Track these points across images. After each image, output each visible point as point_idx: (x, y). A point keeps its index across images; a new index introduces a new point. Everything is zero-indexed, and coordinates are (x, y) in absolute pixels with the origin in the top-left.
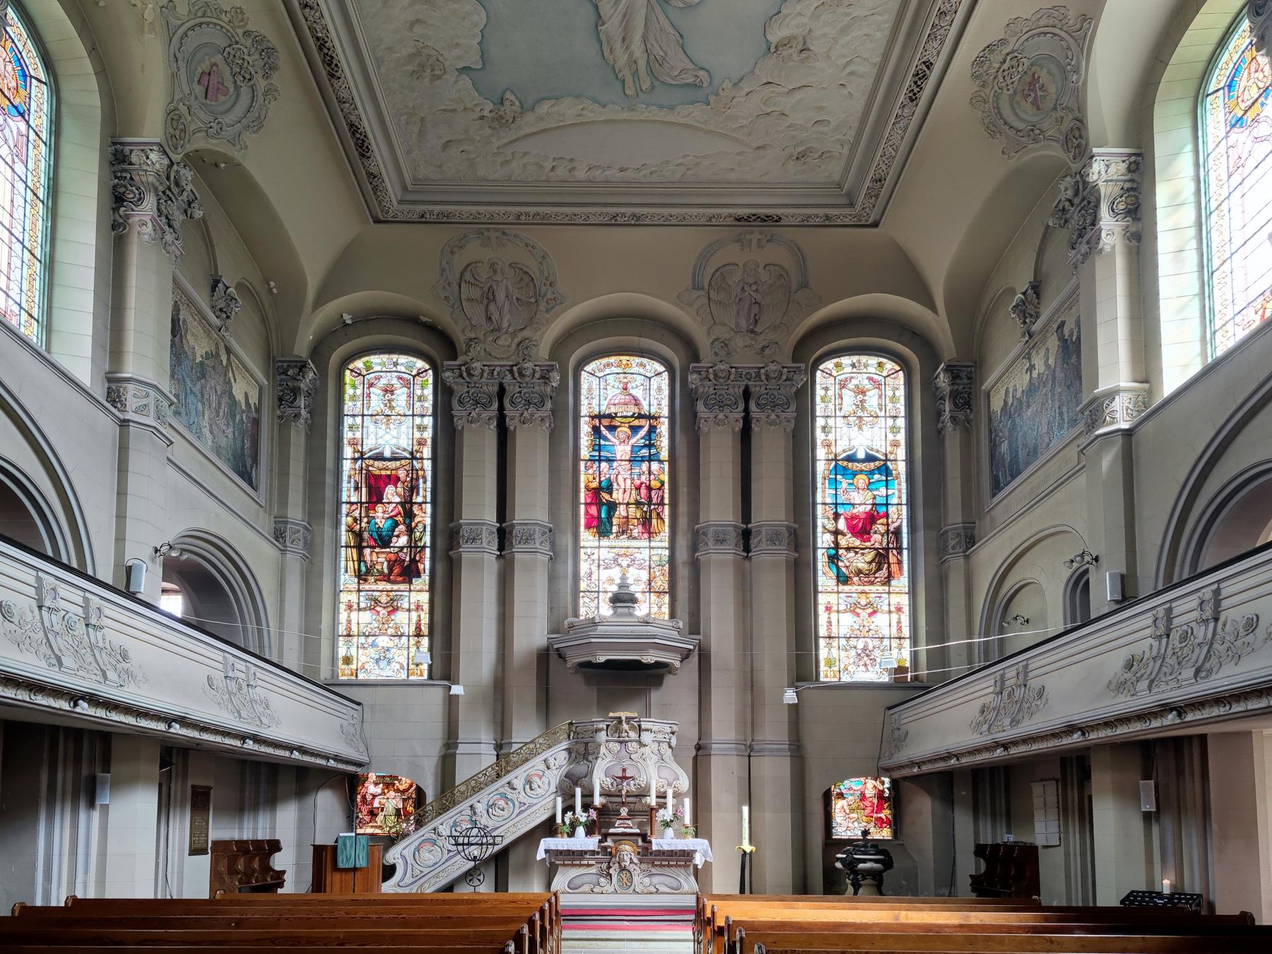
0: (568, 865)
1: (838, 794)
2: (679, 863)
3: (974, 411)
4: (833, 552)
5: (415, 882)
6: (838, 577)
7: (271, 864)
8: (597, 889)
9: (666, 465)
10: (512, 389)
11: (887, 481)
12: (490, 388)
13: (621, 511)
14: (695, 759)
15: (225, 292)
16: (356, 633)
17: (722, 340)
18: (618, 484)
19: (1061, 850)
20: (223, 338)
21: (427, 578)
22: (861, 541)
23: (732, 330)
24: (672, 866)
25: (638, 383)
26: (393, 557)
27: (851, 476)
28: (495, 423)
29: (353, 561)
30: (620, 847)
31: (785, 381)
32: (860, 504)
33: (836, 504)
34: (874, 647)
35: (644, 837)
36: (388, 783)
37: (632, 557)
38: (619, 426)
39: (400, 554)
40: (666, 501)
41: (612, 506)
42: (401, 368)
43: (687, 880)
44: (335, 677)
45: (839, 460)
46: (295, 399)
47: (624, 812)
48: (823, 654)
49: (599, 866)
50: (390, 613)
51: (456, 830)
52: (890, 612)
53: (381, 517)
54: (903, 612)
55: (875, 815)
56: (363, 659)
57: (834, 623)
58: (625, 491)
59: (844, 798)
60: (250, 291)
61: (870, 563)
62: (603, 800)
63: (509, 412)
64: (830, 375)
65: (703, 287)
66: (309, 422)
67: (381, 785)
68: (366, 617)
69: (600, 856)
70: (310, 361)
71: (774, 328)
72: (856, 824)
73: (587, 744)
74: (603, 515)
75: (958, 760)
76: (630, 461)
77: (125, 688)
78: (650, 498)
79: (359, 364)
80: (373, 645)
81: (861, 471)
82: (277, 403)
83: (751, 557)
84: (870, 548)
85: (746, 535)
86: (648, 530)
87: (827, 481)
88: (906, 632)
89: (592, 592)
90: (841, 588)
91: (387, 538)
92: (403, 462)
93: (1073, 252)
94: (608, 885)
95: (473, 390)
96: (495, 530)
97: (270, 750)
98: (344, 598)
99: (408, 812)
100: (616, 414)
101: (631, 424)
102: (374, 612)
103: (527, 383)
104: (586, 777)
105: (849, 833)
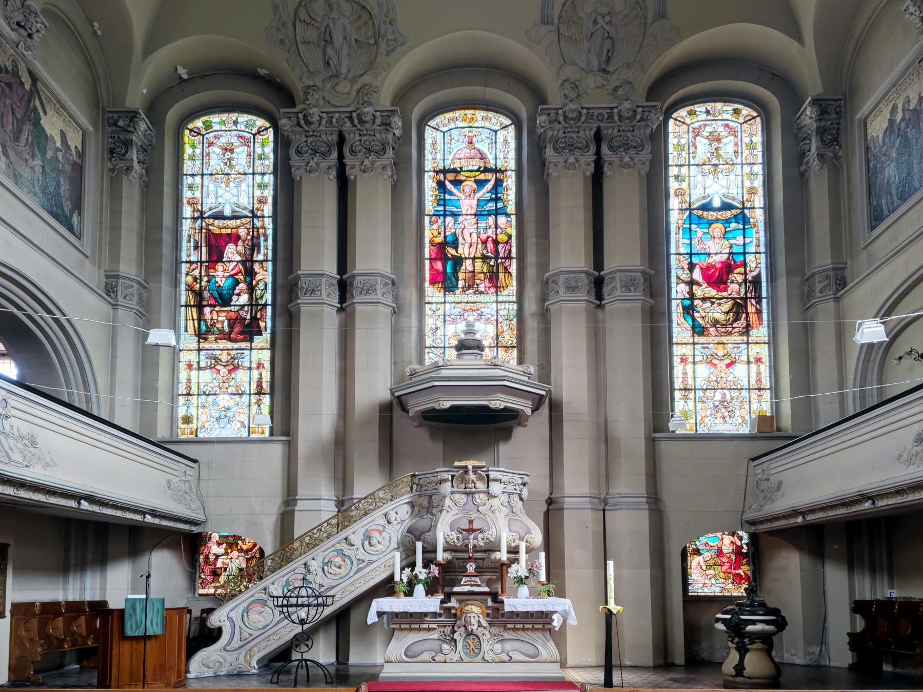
0: (405, 629)
1: (694, 550)
2: (536, 626)
3: (844, 146)
4: (688, 303)
5: (244, 645)
6: (693, 328)
8: (439, 657)
9: (513, 218)
10: (352, 138)
11: (744, 229)
13: (468, 265)
14: (547, 514)
16: (196, 393)
17: (573, 81)
18: (463, 238)
20: (24, 57)
21: (269, 336)
22: (718, 292)
23: (583, 69)
24: (528, 629)
25: (484, 137)
26: (233, 316)
27: (707, 225)
28: (335, 173)
29: (193, 320)
30: (467, 608)
31: (639, 121)
32: (716, 254)
33: (691, 254)
34: (732, 399)
35: (494, 596)
36: (231, 542)
37: (479, 312)
38: (465, 181)
40: (514, 254)
41: (458, 261)
42: (239, 127)
43: (545, 646)
44: (174, 435)
46: (126, 152)
47: (471, 567)
49: (442, 629)
50: (230, 372)
52: (749, 362)
54: (762, 362)
55: (733, 571)
56: (203, 418)
57: (690, 375)
59: (700, 554)
60: (66, 23)
61: (727, 313)
62: (448, 556)
63: (349, 160)
64: (683, 123)
65: (553, 20)
67: (224, 545)
68: (206, 375)
69: (443, 619)
71: (628, 66)
72: (713, 580)
73: (430, 497)
74: (449, 270)
75: (873, 503)
76: (475, 215)
77: (31, 469)
78: (497, 252)
79: (199, 123)
80: (215, 403)
81: (717, 220)
82: (107, 156)
83: (604, 305)
84: (727, 298)
85: (598, 284)
87: (681, 231)
88: (766, 383)
89: (437, 347)
90: (697, 339)
91: (227, 297)
92: (243, 220)
94: (453, 653)
96: (335, 282)
97: (119, 513)
100: (461, 168)
101: (477, 178)
102: (214, 370)
103: (367, 130)
104: (429, 531)
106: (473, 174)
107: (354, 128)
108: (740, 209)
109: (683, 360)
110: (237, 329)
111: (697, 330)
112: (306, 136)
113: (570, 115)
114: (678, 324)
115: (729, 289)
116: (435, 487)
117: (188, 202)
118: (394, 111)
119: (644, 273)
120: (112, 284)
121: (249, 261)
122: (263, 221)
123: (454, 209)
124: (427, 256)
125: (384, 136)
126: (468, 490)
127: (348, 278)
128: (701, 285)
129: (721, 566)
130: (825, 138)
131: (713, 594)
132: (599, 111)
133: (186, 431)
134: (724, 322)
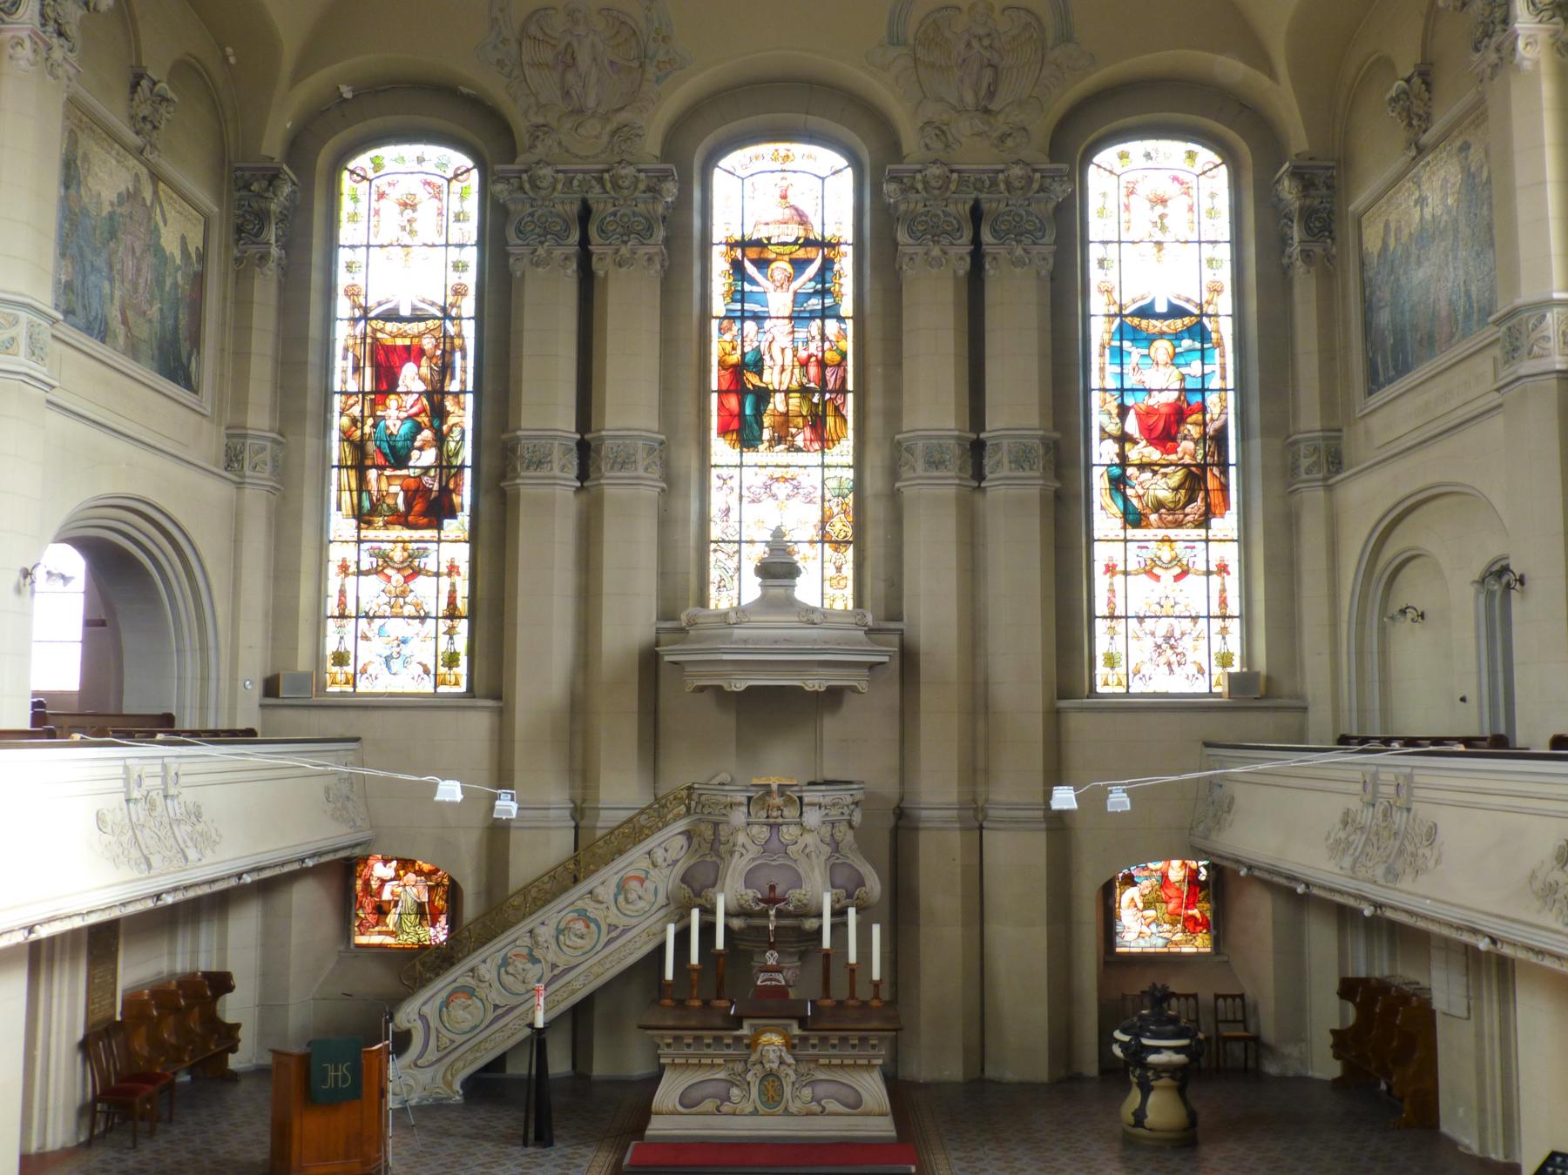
4: (1116, 471)
6: (1125, 513)
7: (219, 1014)
8: (727, 1107)
9: (850, 324)
10: (601, 208)
11: (1202, 350)
12: (568, 208)
13: (778, 402)
15: (151, 91)
16: (354, 614)
18: (771, 357)
19: (1470, 1026)
23: (954, 108)
26: (412, 484)
27: (1145, 343)
28: (575, 266)
29: (350, 491)
31: (1038, 192)
32: (1161, 391)
34: (1183, 634)
37: (795, 482)
39: (425, 479)
40: (850, 386)
41: (763, 395)
42: (426, 167)
45: (1126, 316)
46: (261, 230)
48: (1102, 645)
50: (407, 579)
51: (507, 973)
52: (1208, 573)
53: (395, 417)
54: (1228, 573)
58: (783, 370)
59: (1134, 884)
61: (1176, 490)
66: (284, 262)
67: (394, 863)
68: (372, 584)
70: (285, 168)
72: (1153, 927)
73: (716, 824)
76: (791, 318)
78: (823, 381)
81: (1162, 335)
84: (1177, 465)
85: (976, 450)
86: (823, 439)
87: (1107, 352)
88: (1234, 607)
89: (729, 542)
90: (1133, 533)
92: (430, 323)
93: (1478, 55)
95: (540, 212)
96: (573, 445)
98: (336, 553)
99: (436, 908)
100: (769, 239)
101: (794, 256)
105: (1142, 942)
106: (788, 249)
107: (606, 195)
108: (1196, 316)
109: (1110, 569)
110: (417, 508)
111: (1131, 517)
112: (532, 206)
113: (933, 183)
114: (1102, 508)
115: (1179, 449)
116: (723, 811)
117: (346, 291)
118: (666, 170)
119: (1043, 440)
120: (235, 449)
121: (437, 393)
122: (460, 325)
123: (757, 308)
124: (714, 386)
125: (651, 207)
126: (772, 820)
127: (593, 439)
128: (1137, 443)
129: (1167, 903)
130: (1311, 225)
131: (1152, 950)
132: (978, 176)
133: (338, 678)
134: (1172, 506)
